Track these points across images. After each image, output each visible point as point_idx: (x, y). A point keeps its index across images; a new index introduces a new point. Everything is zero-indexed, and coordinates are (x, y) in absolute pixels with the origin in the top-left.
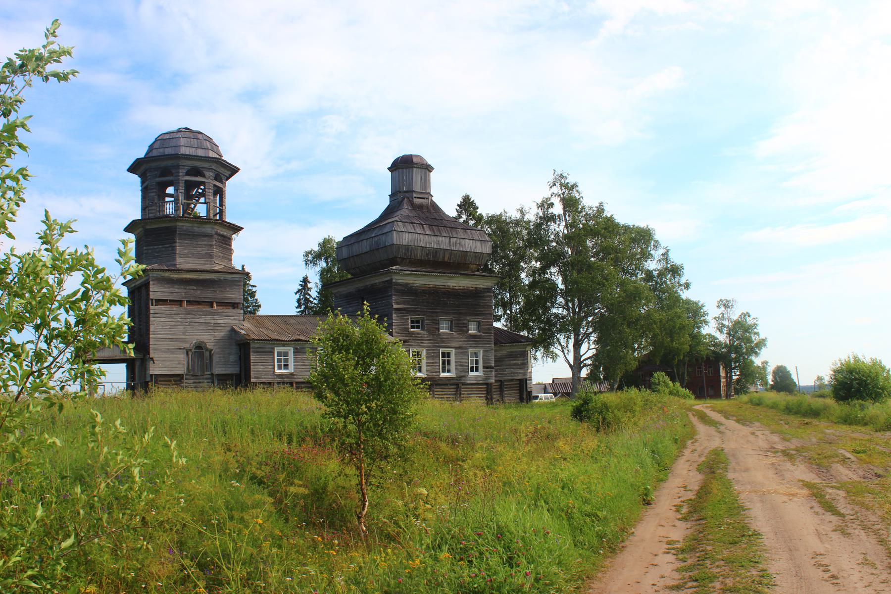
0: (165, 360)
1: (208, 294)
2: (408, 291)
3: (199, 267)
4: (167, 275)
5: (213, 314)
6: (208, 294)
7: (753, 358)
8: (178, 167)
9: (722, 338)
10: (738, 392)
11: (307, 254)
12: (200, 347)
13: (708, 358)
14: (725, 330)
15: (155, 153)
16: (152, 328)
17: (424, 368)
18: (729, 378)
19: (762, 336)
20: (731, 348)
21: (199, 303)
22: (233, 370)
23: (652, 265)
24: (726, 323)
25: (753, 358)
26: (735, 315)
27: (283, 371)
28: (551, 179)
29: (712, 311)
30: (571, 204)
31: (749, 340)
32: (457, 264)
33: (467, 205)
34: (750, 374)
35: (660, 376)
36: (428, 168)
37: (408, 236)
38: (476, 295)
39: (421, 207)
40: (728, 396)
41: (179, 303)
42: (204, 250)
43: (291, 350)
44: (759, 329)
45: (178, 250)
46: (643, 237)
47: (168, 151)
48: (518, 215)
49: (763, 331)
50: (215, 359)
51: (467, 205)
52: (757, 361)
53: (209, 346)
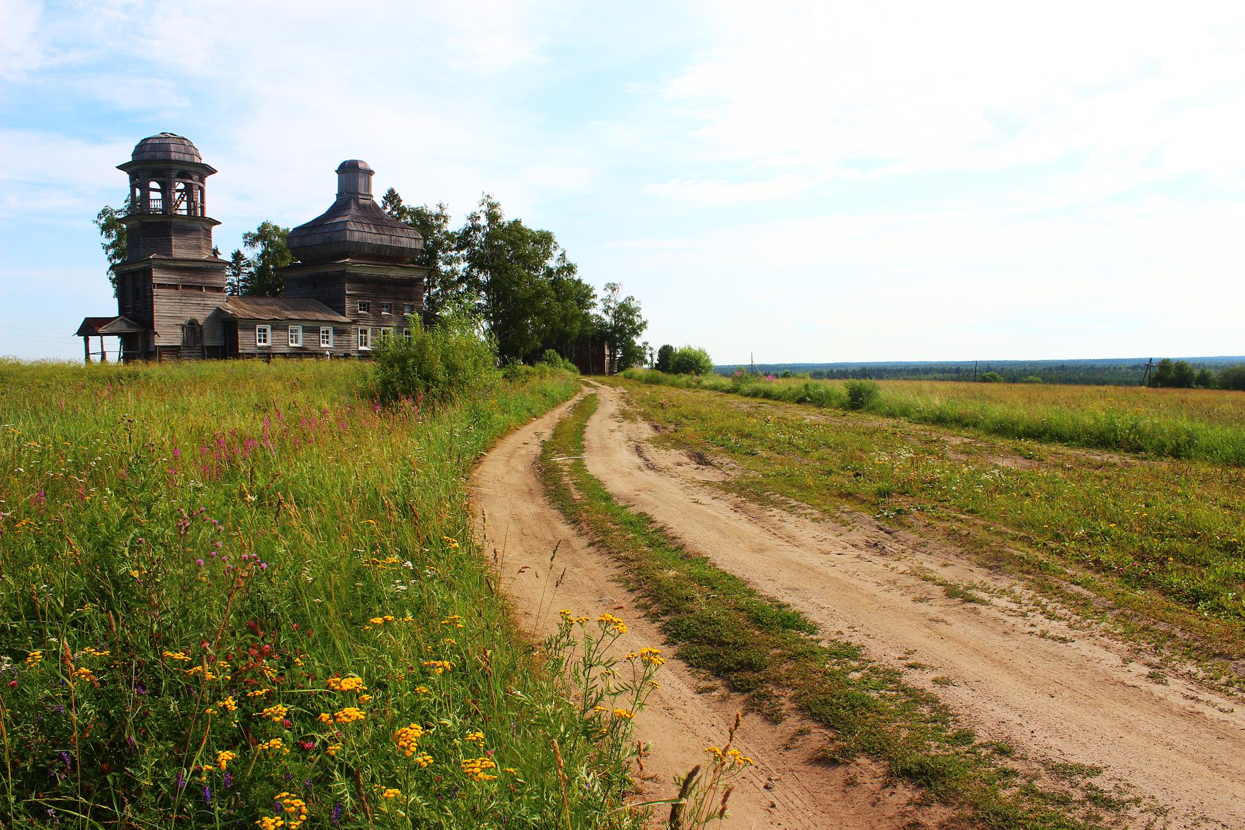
0: (167, 334)
1: (198, 280)
2: (357, 279)
3: (191, 257)
4: (165, 263)
5: (201, 296)
6: (198, 280)
7: (634, 338)
8: (170, 170)
9: (608, 319)
10: (620, 369)
11: (246, 236)
12: (192, 324)
13: (593, 337)
14: (611, 312)
15: (146, 156)
16: (155, 307)
17: (369, 343)
18: (613, 356)
19: (644, 319)
20: (615, 329)
21: (191, 287)
22: (219, 343)
23: (552, 263)
24: (612, 305)
25: (634, 338)
26: (621, 298)
27: (262, 344)
28: (480, 198)
29: (600, 293)
30: (493, 217)
31: (631, 322)
32: (396, 256)
33: (392, 197)
34: (633, 355)
35: (550, 352)
36: (370, 173)
37: (359, 233)
38: (412, 283)
39: (365, 206)
40: (611, 373)
41: (176, 287)
42: (194, 242)
43: (269, 328)
44: (641, 313)
45: (174, 242)
46: (545, 239)
47: (160, 155)
48: (438, 210)
49: (645, 314)
50: (205, 333)
51: (392, 197)
52: (638, 341)
53: (201, 322)
